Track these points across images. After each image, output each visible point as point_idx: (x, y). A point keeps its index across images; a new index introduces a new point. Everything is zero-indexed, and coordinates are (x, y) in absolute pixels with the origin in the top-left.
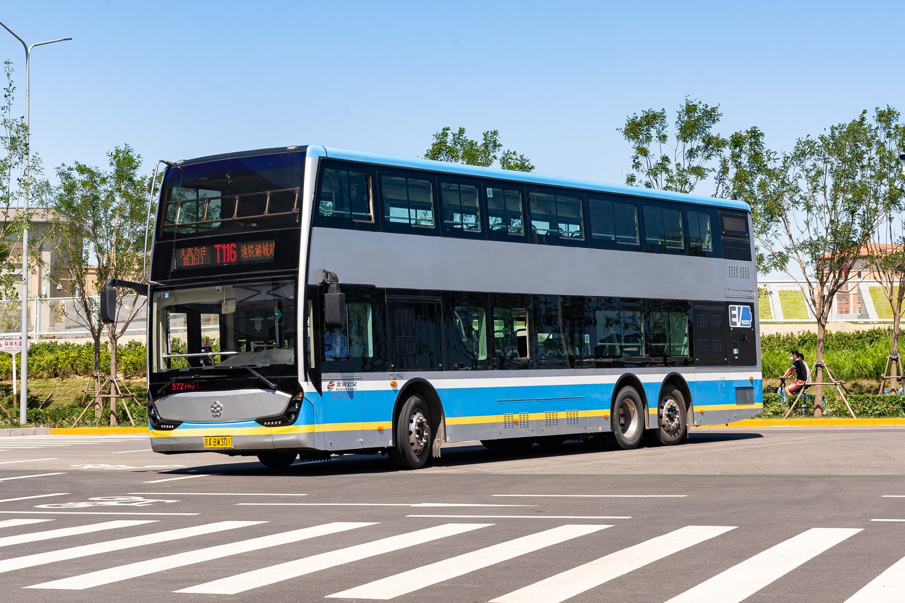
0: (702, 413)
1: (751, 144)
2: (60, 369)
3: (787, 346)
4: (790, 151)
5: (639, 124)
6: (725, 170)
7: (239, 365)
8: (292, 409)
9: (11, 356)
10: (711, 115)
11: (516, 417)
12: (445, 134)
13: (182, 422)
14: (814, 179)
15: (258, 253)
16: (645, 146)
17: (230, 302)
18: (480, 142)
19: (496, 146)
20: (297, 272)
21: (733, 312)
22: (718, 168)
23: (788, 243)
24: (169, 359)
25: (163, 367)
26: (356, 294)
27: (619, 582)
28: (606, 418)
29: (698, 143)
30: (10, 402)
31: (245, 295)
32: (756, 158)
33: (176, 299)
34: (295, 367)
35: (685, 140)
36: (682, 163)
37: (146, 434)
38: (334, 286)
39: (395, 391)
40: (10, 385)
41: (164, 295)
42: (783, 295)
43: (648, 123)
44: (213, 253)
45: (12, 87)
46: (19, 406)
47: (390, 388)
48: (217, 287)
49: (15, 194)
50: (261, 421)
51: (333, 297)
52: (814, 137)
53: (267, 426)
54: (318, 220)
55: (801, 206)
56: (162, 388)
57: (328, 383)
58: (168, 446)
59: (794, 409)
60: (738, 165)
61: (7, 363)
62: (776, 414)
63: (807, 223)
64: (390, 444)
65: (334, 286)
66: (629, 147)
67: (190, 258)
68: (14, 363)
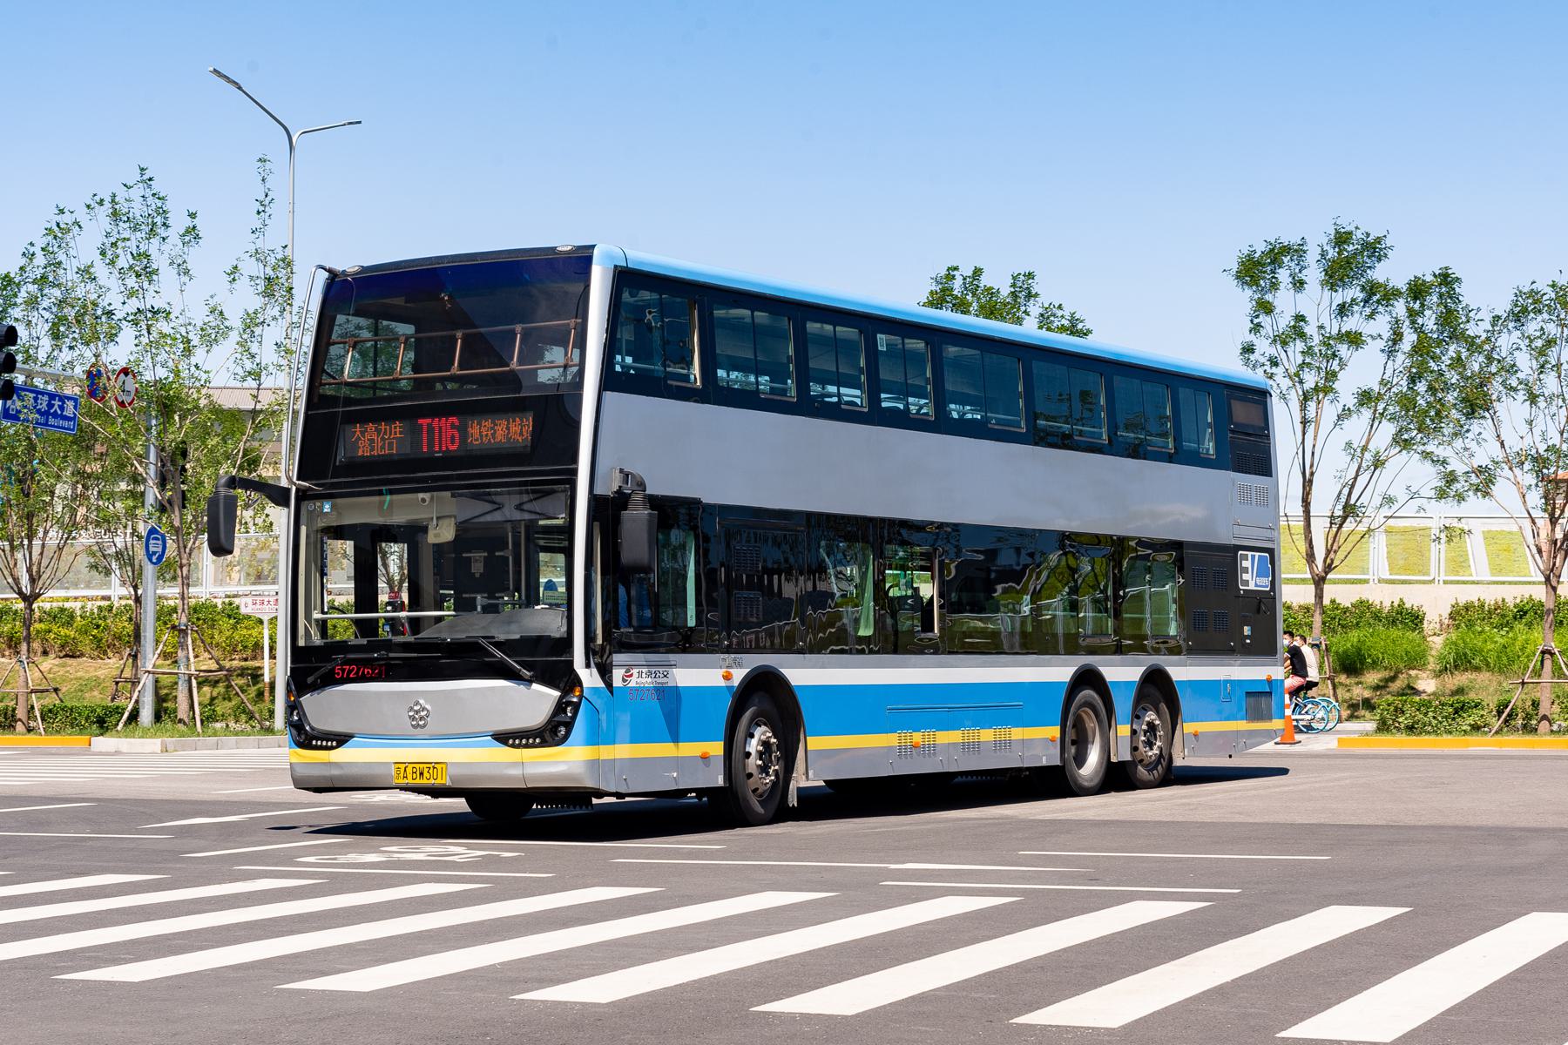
1: (1441, 296)
3: (1495, 619)
4: (1503, 307)
5: (1259, 263)
6: (1397, 337)
7: (461, 636)
8: (561, 718)
9: (261, 622)
10: (1374, 249)
11: (917, 737)
12: (951, 278)
13: (351, 736)
14: (1542, 352)
16: (1269, 297)
17: (445, 522)
18: (1005, 291)
19: (1030, 296)
20: (575, 472)
22: (1386, 334)
23: (1499, 454)
24: (324, 622)
25: (317, 640)
27: (1220, 993)
28: (1053, 740)
29: (1353, 292)
30: (260, 694)
31: (473, 509)
32: (1449, 319)
33: (340, 514)
34: (566, 643)
35: (1333, 288)
36: (1327, 325)
37: (281, 753)
38: (638, 497)
40: (260, 668)
41: (322, 507)
42: (1490, 537)
43: (1273, 262)
44: (415, 432)
46: (273, 701)
47: (722, 683)
48: (421, 495)
49: (271, 368)
50: (503, 738)
51: (637, 517)
52: (1543, 286)
53: (513, 746)
54: (611, 381)
55: (1521, 396)
56: (318, 674)
57: (622, 671)
58: (324, 777)
59: (1506, 721)
60: (1419, 330)
61: (254, 633)
62: (1476, 728)
63: (1530, 423)
64: (720, 781)
65: (638, 497)
66: (1245, 298)
67: (370, 441)
68: (266, 633)
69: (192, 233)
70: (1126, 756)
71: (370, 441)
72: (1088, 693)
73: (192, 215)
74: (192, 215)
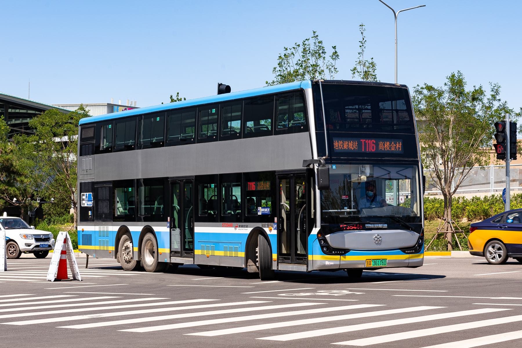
2: (428, 214)
45: (364, 40)
50: (404, 250)
53: (407, 253)
69: (335, 56)
73: (334, 48)
74: (334, 48)
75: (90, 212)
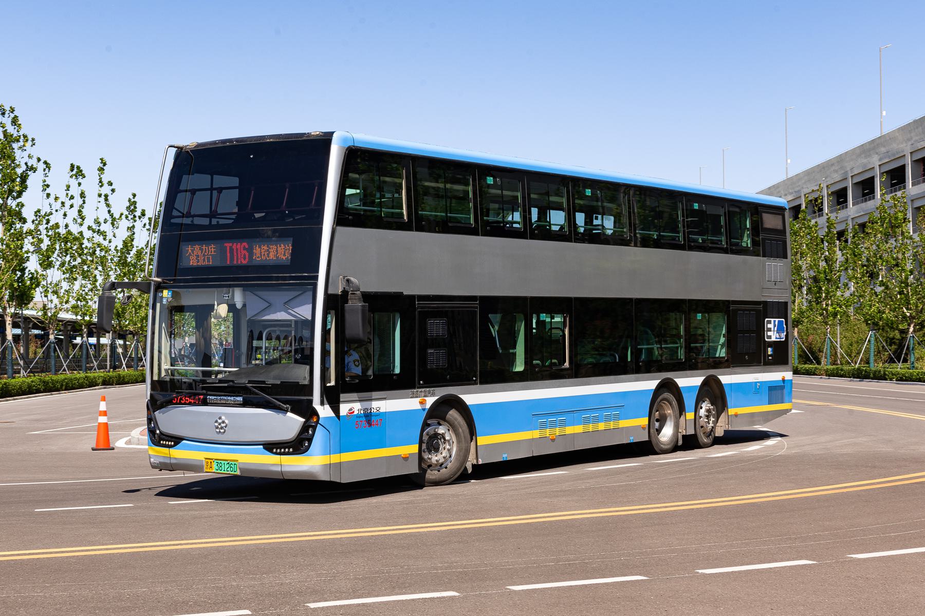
0: (736, 415)
8: (304, 436)
15: (272, 256)
20: (316, 278)
21: (769, 326)
26: (382, 304)
28: (644, 428)
34: (309, 389)
39: (424, 410)
47: (419, 407)
50: (271, 447)
51: (355, 304)
53: (276, 453)
54: (343, 218)
67: (197, 255)
70: (691, 431)
71: (197, 255)
72: (667, 395)
75: (770, 349)
